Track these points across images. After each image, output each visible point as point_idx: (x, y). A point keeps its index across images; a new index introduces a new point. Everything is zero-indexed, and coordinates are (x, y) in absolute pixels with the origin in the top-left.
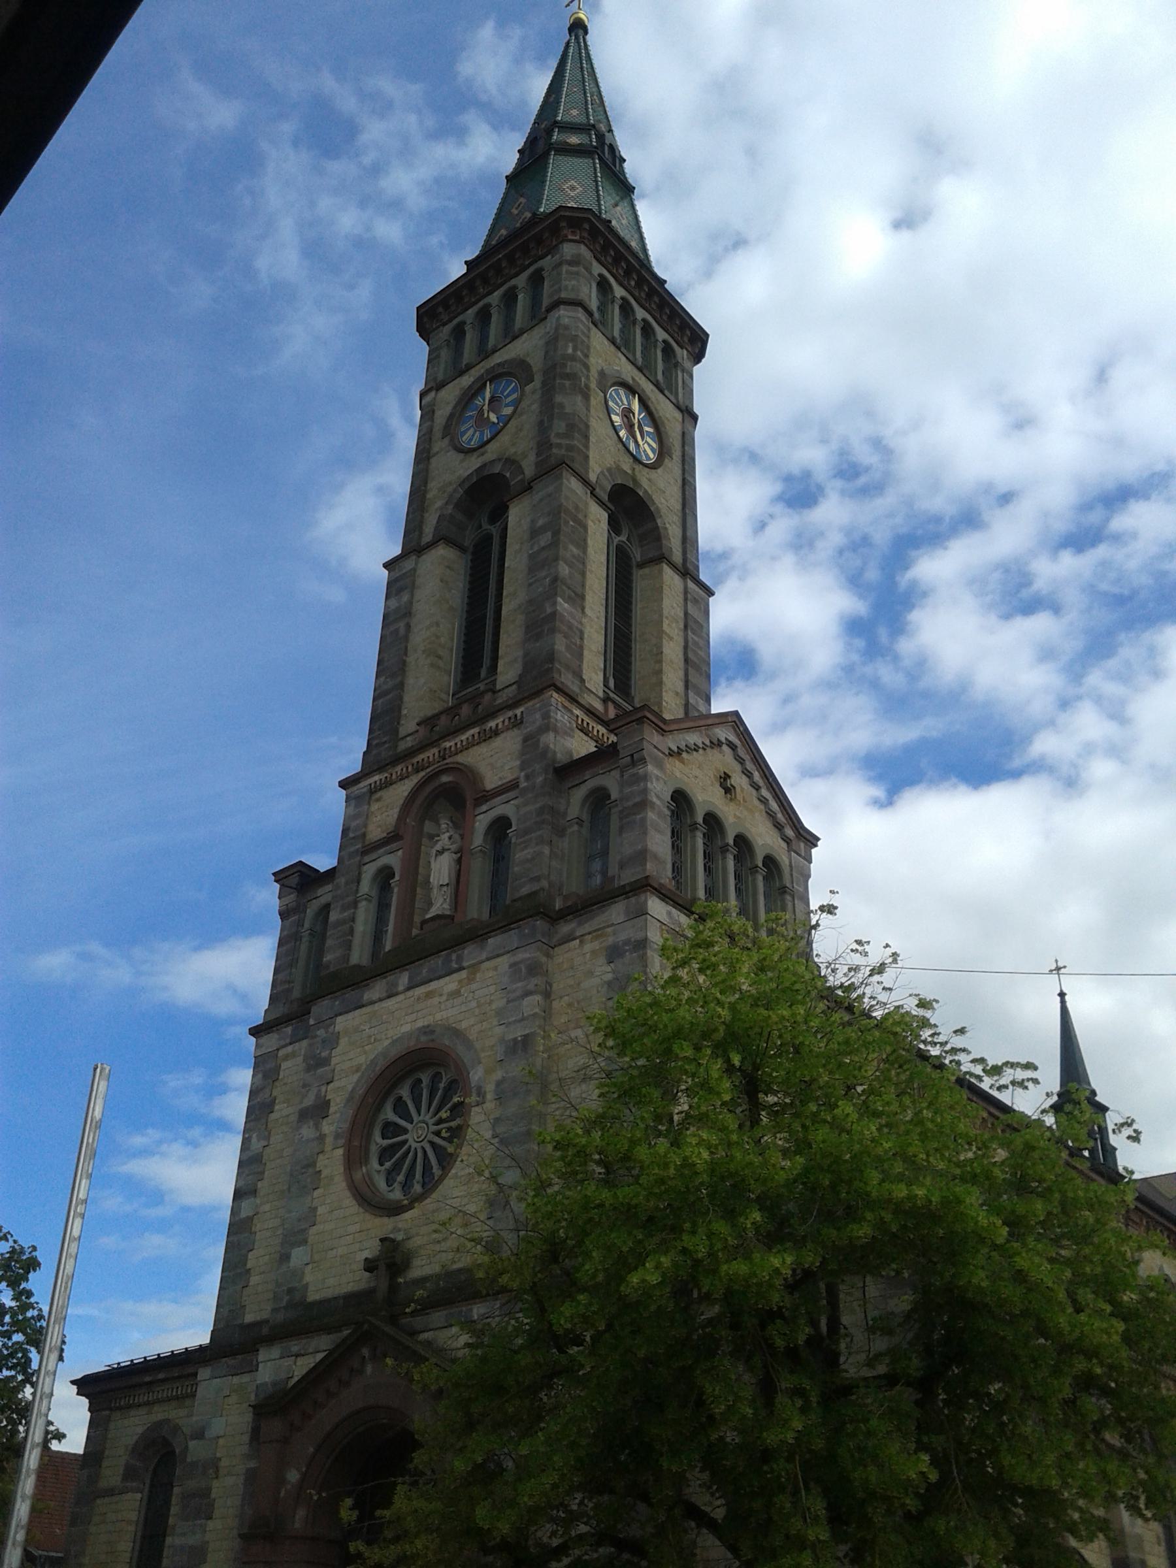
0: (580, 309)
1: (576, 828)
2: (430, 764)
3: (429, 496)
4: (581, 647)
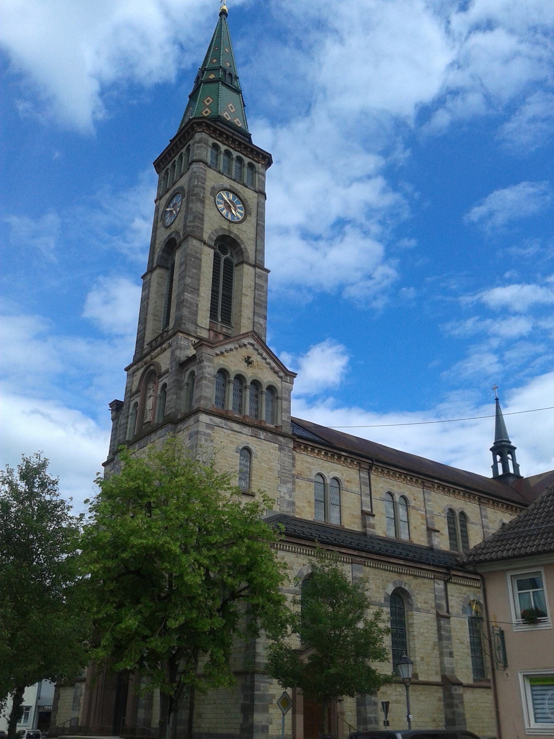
0: (201, 163)
1: (186, 387)
2: (148, 362)
3: (156, 246)
4: (197, 311)
